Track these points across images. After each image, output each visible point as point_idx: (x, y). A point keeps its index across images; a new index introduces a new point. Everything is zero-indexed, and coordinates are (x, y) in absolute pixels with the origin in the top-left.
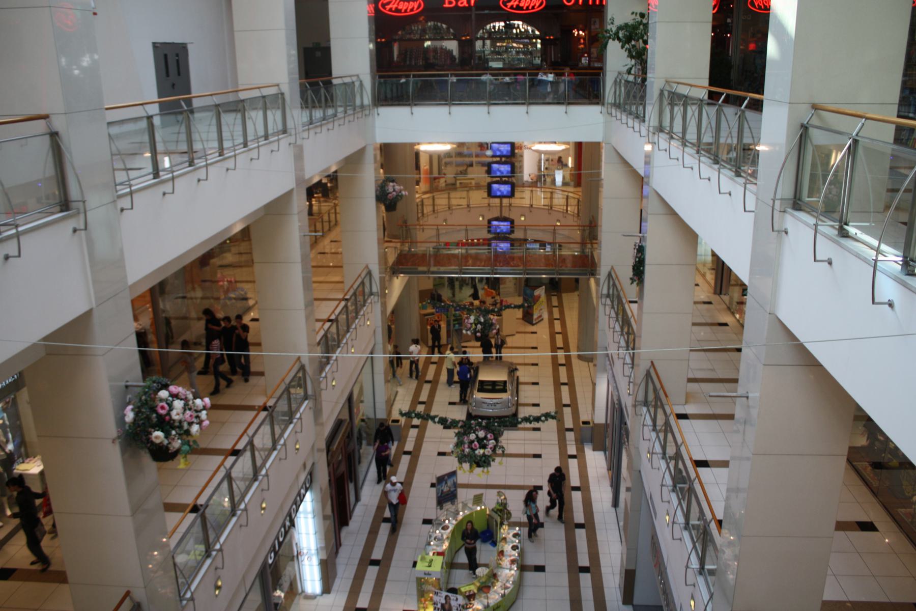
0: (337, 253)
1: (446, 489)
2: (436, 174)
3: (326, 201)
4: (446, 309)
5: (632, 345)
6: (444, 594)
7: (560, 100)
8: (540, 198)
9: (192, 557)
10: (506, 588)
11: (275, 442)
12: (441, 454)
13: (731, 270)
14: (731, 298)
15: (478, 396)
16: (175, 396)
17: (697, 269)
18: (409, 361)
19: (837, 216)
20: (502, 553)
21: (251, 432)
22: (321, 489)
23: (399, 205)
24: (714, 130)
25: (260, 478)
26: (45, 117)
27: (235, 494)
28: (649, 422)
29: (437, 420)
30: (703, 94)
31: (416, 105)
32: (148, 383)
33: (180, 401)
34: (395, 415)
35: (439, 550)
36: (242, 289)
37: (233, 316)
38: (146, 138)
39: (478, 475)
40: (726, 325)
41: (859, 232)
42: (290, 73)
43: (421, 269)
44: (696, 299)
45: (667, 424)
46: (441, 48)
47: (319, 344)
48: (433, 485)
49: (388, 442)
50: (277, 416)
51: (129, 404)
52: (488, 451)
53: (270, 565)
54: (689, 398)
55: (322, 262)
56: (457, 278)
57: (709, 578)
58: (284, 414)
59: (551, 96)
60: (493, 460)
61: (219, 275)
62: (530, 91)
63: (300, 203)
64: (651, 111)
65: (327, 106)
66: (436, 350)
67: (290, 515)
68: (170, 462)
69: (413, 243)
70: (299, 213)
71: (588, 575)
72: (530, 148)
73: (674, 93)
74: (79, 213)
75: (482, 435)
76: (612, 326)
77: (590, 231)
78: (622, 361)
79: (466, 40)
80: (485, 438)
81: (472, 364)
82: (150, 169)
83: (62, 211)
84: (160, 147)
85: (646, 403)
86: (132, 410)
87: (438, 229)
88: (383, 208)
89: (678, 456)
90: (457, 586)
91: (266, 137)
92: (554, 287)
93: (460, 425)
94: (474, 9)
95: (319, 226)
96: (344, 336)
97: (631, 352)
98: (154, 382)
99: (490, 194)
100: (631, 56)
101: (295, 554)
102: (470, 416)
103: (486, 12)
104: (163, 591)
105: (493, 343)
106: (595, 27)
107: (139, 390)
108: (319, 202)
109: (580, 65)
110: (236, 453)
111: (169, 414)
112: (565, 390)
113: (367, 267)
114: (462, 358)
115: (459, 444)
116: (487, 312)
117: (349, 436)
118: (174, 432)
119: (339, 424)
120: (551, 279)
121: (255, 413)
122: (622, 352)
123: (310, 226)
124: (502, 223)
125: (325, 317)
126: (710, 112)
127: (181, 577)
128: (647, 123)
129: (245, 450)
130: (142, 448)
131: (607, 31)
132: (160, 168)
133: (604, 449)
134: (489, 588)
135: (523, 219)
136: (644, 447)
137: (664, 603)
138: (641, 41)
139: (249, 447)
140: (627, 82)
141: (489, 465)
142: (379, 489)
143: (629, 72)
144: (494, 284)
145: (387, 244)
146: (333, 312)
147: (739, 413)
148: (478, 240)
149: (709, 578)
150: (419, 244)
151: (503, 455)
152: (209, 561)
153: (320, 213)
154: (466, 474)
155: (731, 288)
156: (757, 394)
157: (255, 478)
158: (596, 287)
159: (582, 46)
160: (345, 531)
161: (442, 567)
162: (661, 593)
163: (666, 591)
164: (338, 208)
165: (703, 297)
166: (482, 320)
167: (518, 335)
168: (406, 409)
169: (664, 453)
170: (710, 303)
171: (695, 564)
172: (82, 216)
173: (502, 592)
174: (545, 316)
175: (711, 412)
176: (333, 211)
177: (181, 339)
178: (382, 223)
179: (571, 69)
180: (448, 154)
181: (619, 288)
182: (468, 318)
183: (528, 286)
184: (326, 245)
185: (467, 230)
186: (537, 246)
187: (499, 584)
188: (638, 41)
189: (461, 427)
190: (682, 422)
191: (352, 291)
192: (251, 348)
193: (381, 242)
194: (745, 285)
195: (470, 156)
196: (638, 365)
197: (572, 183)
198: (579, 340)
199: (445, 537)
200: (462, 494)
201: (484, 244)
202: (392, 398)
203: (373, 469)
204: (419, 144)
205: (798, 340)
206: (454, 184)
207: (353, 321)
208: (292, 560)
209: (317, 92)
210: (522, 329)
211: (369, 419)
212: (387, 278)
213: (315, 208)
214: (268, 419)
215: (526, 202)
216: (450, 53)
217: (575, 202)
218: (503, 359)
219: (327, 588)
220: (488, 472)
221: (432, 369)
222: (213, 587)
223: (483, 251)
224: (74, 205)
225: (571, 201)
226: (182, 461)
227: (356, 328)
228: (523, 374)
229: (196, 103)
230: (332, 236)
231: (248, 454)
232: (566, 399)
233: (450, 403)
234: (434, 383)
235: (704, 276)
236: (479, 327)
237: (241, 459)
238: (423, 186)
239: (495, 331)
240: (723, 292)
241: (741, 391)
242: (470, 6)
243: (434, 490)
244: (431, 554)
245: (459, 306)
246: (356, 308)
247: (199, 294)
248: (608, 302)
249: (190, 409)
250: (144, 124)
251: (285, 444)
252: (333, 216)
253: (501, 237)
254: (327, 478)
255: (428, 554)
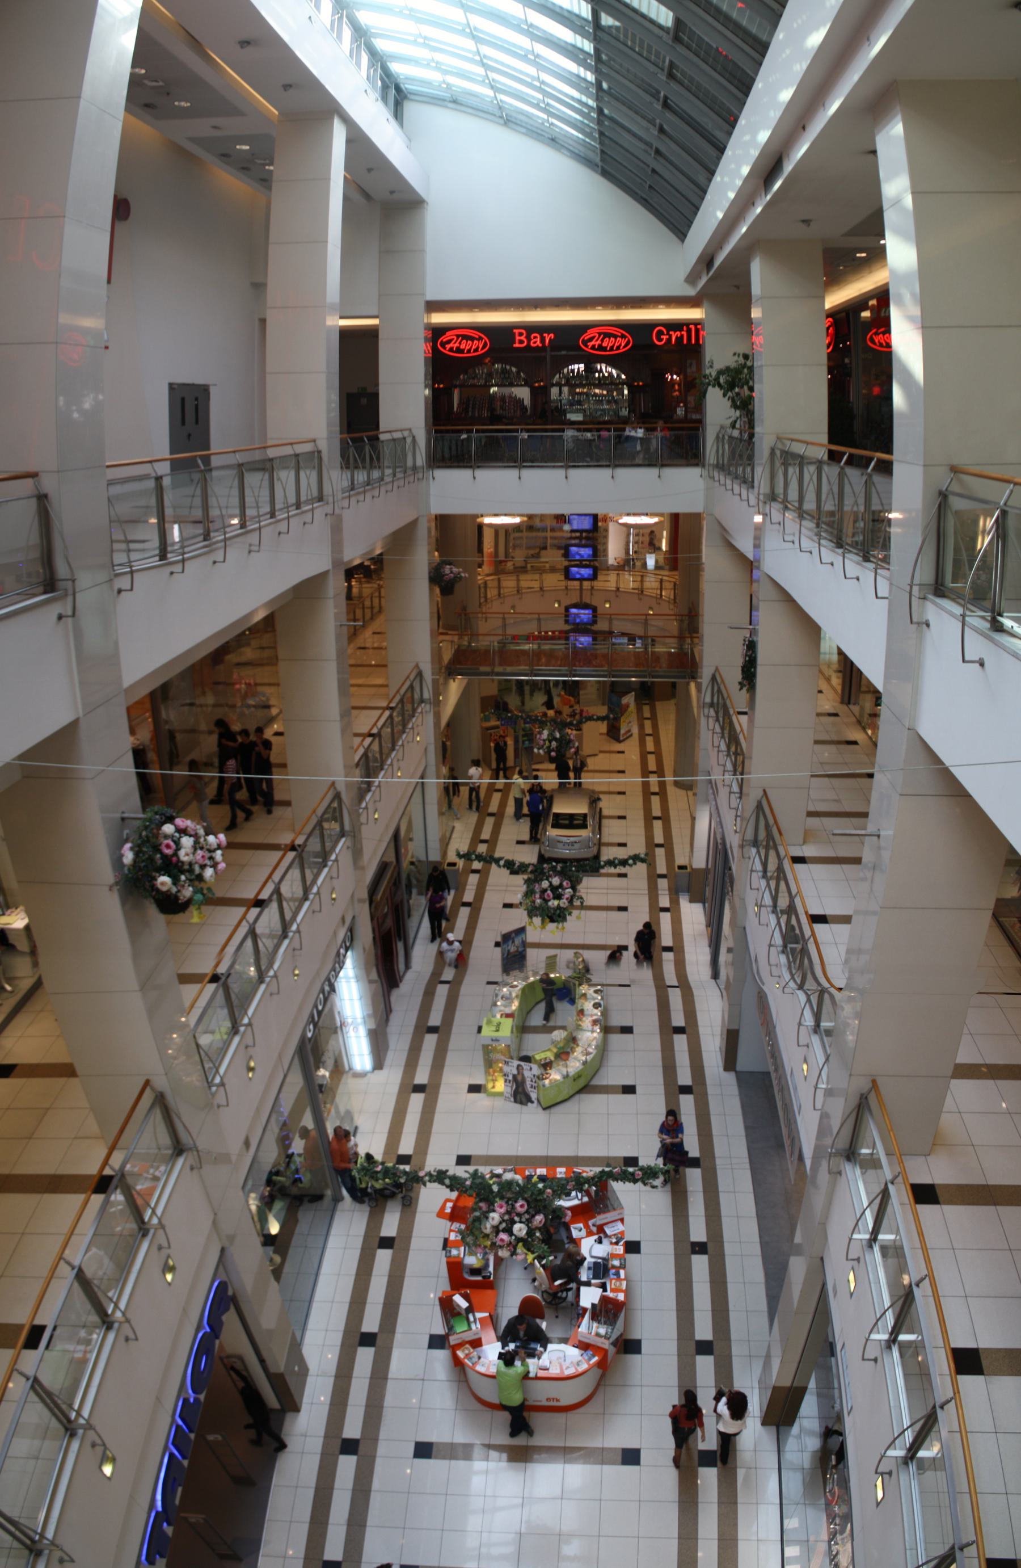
0: (380, 648)
1: (513, 949)
2: (502, 557)
3: (368, 582)
4: (513, 721)
5: (740, 769)
6: (516, 1063)
7: (652, 461)
8: (629, 581)
9: (217, 1036)
10: (588, 1054)
11: (306, 890)
12: (507, 906)
13: (861, 673)
14: (862, 709)
15: (553, 833)
16: (183, 831)
17: (821, 672)
18: (468, 788)
19: (988, 604)
20: (581, 1012)
21: (276, 877)
22: (364, 949)
23: (458, 587)
24: (836, 496)
25: (291, 934)
26: (34, 475)
27: (262, 955)
28: (758, 866)
29: (502, 863)
30: (822, 453)
31: (478, 467)
32: (149, 815)
33: (188, 838)
34: (452, 857)
35: (508, 1011)
36: (264, 695)
37: (252, 729)
38: (153, 502)
39: (551, 932)
40: (855, 743)
41: (1015, 625)
42: (329, 425)
43: (483, 669)
44: (819, 711)
45: (780, 869)
46: (510, 397)
47: (357, 765)
48: (497, 944)
49: (443, 891)
50: (309, 858)
51: (126, 841)
52: (564, 903)
53: (310, 1039)
54: (808, 837)
55: (362, 661)
56: (527, 681)
57: (825, 1038)
58: (316, 855)
59: (641, 456)
60: (570, 914)
61: (235, 676)
62: (615, 449)
63: (336, 585)
64: (761, 473)
65: (372, 467)
66: (501, 773)
67: (328, 980)
68: (181, 915)
69: (474, 635)
70: (335, 596)
71: (684, 1037)
72: (617, 522)
73: (787, 453)
74: (66, 595)
75: (556, 881)
76: (716, 744)
77: (690, 622)
78: (727, 789)
79: (540, 387)
80: (561, 886)
81: (544, 792)
82: (156, 543)
83: (45, 593)
84: (169, 512)
85: (755, 843)
86: (131, 849)
87: (504, 619)
88: (437, 590)
89: (791, 910)
90: (530, 1054)
91: (298, 505)
92: (647, 693)
93: (529, 870)
94: (548, 349)
95: (359, 613)
96: (388, 755)
97: (740, 777)
98: (156, 813)
99: (568, 576)
100: (735, 406)
101: (338, 1024)
102: (542, 858)
103: (564, 353)
104: (189, 1079)
105: (571, 765)
106: (691, 370)
107: (138, 823)
108: (360, 583)
109: (675, 417)
110: (259, 903)
111: (176, 854)
112: (658, 825)
113: (417, 666)
114: (533, 785)
115: (529, 893)
116: (563, 725)
117: (396, 883)
118: (183, 878)
119: (383, 867)
120: (643, 683)
121: (280, 853)
122: (728, 777)
123: (348, 613)
124: (582, 611)
125: (365, 730)
126: (831, 471)
127: (207, 1060)
128: (756, 490)
129: (270, 899)
130: (146, 897)
131: (705, 376)
132: (169, 542)
133: (702, 900)
134: (568, 1054)
135: (607, 606)
136: (751, 897)
137: (772, 1069)
138: (746, 387)
139: (275, 897)
140: (731, 437)
141: (564, 919)
142: (433, 948)
143: (733, 426)
144: (573, 689)
145: (442, 637)
146: (375, 724)
147: (867, 856)
148: (553, 632)
149: (825, 1038)
150: (481, 638)
151: (582, 907)
152: (236, 1040)
153: (360, 596)
154: (537, 931)
155: (862, 696)
156: (891, 832)
157: (284, 935)
158: (698, 693)
159: (677, 393)
160: (395, 994)
161: (512, 1032)
162: (768, 1056)
163: (775, 1054)
164: (382, 590)
165: (827, 707)
166: (558, 735)
167: (601, 755)
168: (464, 849)
169: (775, 906)
170: (836, 715)
171: (809, 1020)
172: (70, 599)
173: (584, 1058)
174: (635, 730)
175: (833, 855)
176: (377, 594)
177: (188, 759)
178: (435, 610)
179: (665, 423)
180: (517, 528)
181: (725, 695)
182: (540, 733)
183: (614, 692)
184: (367, 637)
185: (539, 620)
186: (625, 640)
187: (579, 1050)
188: (742, 387)
189: (531, 872)
190: (798, 867)
191: (397, 698)
192: (274, 770)
193: (435, 634)
194: (879, 692)
195: (544, 529)
196: (748, 795)
197: (667, 567)
198: (676, 762)
199: (514, 995)
200: (531, 954)
201: (560, 638)
202: (448, 835)
203: (426, 923)
204: (482, 516)
205: (942, 763)
206: (525, 567)
207: (400, 736)
208: (335, 1032)
209: (360, 451)
210: (606, 748)
211: (419, 861)
212: (441, 681)
213: (355, 591)
214: (297, 861)
215: (612, 585)
216: (520, 402)
217: (671, 586)
218: (583, 786)
219: (379, 1064)
220: (563, 928)
221: (496, 797)
222: (245, 1070)
223: (559, 646)
224: (61, 585)
225: (665, 585)
226: (195, 913)
227: (403, 745)
228: (608, 806)
229: (215, 461)
230: (375, 626)
231: (274, 905)
232: (659, 839)
233: (519, 842)
234: (499, 816)
235: (828, 679)
236: (554, 744)
237: (266, 911)
238: (486, 569)
239: (573, 750)
240: (852, 701)
241: (871, 828)
242: (544, 347)
243: (499, 949)
244: (498, 1016)
245: (529, 717)
246: (403, 719)
247: (210, 700)
248: (712, 712)
249: (202, 848)
250: (151, 484)
251: (318, 893)
252: (376, 601)
253: (581, 629)
254: (370, 936)
255: (494, 1016)
